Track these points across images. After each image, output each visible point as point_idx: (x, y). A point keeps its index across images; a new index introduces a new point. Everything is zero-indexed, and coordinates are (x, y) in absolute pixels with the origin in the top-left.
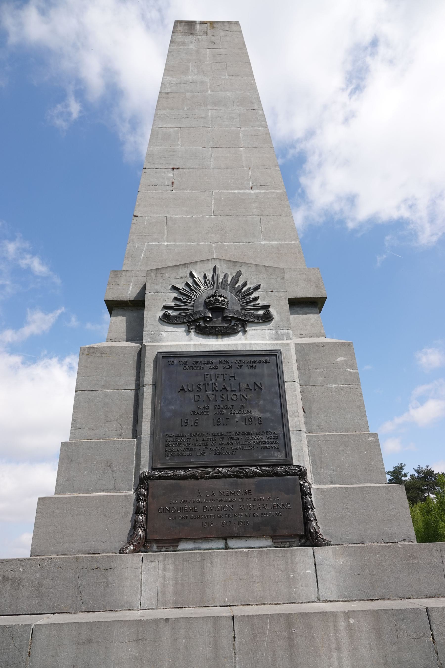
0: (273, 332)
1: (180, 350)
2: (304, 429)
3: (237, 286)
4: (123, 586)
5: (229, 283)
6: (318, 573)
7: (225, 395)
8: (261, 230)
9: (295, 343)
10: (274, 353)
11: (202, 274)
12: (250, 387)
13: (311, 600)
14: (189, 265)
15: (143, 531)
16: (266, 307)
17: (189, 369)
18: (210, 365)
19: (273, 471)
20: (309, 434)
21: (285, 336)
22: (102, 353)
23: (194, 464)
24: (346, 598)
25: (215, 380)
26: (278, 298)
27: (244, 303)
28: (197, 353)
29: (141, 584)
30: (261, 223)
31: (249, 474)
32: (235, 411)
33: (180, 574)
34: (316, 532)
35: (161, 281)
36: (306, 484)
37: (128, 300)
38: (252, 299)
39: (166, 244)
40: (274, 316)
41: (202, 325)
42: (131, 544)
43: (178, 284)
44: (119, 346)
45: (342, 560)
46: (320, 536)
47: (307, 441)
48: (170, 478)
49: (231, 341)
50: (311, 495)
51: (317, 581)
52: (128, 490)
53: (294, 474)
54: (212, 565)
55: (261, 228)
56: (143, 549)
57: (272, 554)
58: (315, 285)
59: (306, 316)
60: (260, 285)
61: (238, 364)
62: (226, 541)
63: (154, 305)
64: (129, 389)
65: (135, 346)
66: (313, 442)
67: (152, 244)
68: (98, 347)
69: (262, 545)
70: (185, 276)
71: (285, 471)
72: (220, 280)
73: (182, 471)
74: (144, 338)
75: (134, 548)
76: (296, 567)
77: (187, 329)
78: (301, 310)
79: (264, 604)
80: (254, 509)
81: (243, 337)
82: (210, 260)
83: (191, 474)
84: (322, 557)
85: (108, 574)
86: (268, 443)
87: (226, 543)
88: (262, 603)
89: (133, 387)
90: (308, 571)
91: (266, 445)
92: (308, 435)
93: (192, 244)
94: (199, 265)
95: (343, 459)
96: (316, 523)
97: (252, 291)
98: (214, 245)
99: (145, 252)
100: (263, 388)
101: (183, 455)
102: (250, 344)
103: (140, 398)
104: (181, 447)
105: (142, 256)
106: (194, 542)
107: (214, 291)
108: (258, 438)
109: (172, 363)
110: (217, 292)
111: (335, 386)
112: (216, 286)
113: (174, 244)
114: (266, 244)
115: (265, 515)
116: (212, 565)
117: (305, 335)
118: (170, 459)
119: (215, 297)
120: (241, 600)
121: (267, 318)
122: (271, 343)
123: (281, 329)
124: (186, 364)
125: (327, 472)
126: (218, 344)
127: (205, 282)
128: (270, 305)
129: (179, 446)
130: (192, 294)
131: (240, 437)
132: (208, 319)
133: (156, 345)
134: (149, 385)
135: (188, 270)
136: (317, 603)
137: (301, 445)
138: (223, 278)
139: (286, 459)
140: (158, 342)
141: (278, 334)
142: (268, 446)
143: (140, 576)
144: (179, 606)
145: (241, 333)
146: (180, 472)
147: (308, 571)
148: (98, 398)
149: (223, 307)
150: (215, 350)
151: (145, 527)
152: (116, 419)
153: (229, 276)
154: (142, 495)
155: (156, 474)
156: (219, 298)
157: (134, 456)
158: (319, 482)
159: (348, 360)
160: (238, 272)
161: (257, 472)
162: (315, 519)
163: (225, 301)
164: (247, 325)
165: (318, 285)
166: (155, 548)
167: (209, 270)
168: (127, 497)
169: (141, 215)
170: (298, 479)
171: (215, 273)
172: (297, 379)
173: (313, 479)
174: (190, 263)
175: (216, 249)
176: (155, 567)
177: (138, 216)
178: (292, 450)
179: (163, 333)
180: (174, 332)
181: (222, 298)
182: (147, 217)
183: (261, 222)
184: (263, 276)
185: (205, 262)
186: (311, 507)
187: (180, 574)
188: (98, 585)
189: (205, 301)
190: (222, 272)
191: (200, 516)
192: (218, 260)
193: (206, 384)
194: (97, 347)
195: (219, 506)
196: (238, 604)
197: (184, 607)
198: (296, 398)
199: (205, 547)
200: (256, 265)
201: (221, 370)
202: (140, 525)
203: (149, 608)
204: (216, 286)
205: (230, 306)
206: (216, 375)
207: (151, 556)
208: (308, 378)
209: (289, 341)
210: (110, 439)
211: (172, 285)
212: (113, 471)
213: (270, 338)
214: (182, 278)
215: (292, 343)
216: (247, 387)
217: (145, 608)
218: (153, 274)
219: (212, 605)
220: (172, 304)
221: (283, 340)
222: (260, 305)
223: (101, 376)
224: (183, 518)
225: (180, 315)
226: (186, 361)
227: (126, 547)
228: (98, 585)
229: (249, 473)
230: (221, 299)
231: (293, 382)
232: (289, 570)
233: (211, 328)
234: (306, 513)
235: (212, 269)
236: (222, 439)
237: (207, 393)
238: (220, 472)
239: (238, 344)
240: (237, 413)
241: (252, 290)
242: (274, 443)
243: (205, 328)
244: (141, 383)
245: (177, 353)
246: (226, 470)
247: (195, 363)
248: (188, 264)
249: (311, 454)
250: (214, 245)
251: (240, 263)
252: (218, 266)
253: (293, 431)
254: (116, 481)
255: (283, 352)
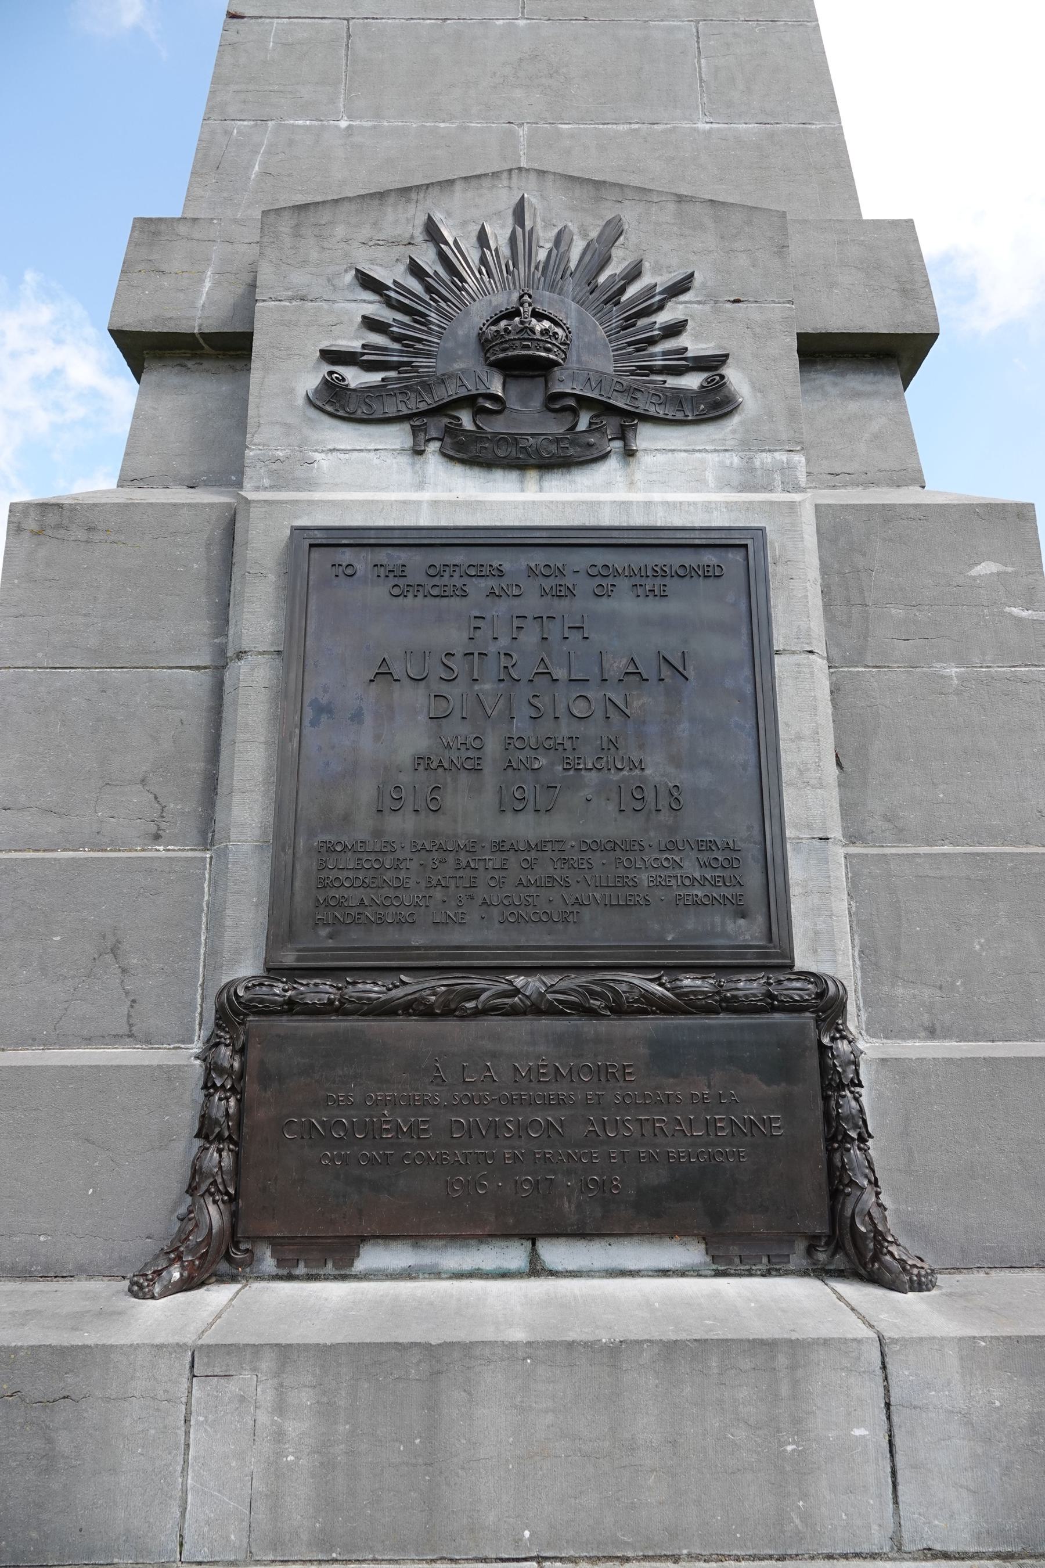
0: (736, 460)
1: (381, 523)
2: (836, 832)
3: (602, 279)
4: (115, 1470)
5: (573, 265)
6: (898, 1441)
7: (547, 699)
8: (700, 76)
9: (817, 506)
10: (737, 542)
11: (469, 229)
12: (641, 670)
13: (865, 1548)
14: (422, 195)
15: (222, 1206)
16: (712, 364)
17: (410, 595)
18: (491, 582)
19: (718, 993)
20: (853, 850)
21: (777, 477)
22: (89, 529)
23: (419, 958)
24: (1009, 1544)
25: (510, 639)
26: (758, 330)
27: (630, 344)
28: (444, 534)
29: (186, 1461)
30: (699, 52)
31: (628, 1002)
32: (581, 761)
33: (343, 1428)
34: (877, 1232)
35: (314, 255)
36: (843, 1046)
37: (196, 331)
38: (660, 329)
39: (343, 124)
40: (740, 400)
41: (467, 428)
42: (174, 1259)
43: (381, 265)
44: (153, 501)
45: (996, 1393)
46: (893, 1249)
47: (847, 878)
48: (327, 1010)
49: (576, 491)
50: (860, 1085)
51: (894, 1473)
52: (178, 1042)
53: (796, 1008)
54: (470, 1394)
55: (700, 68)
56: (223, 1267)
57: (715, 1359)
58: (895, 286)
59: (854, 407)
60: (692, 275)
61: (599, 580)
62: (534, 1244)
63: (288, 349)
64: (190, 668)
65: (212, 505)
66: (868, 881)
67: (293, 125)
68: (77, 504)
69: (666, 1265)
70: (407, 235)
71: (763, 994)
72: (542, 255)
73: (375, 984)
74: (248, 472)
75: (186, 1274)
76: (809, 1413)
77: (409, 442)
78: (835, 384)
79: (676, 1559)
80: (643, 1135)
81: (619, 479)
82: (505, 175)
83: (410, 997)
84: (917, 1375)
85: (52, 1421)
86: (703, 882)
87: (534, 1257)
88: (668, 1553)
89: (204, 660)
90: (858, 1432)
91: (695, 892)
92: (850, 855)
93: (442, 125)
94: (459, 195)
95: (977, 947)
96: (877, 1194)
97: (660, 301)
98: (523, 132)
99: (268, 152)
100: (691, 673)
101: (381, 922)
102: (648, 504)
103: (227, 699)
104: (374, 891)
105: (257, 168)
106: (416, 1246)
107: (515, 296)
108: (665, 864)
109: (349, 571)
110: (526, 298)
111: (958, 670)
112: (522, 276)
113: (375, 127)
114: (718, 129)
115: (683, 1157)
116: (470, 1394)
117: (848, 478)
118: (331, 936)
119: (517, 319)
120: (584, 1539)
121: (716, 405)
122: (727, 499)
123: (762, 451)
124: (399, 572)
125: (917, 992)
126: (524, 502)
127: (483, 261)
128: (727, 356)
129: (364, 885)
130: (430, 305)
131: (597, 858)
132: (488, 406)
133: (286, 502)
134: (260, 653)
135: (418, 214)
136: (890, 1559)
137: (825, 893)
138: (549, 245)
139: (769, 948)
140: (298, 489)
141: (753, 469)
142: (700, 894)
143: (181, 1433)
144: (334, 1555)
145: (613, 463)
146: (369, 987)
147: (858, 1432)
148: (75, 696)
149: (548, 359)
150: (512, 524)
151: (232, 1191)
152: (140, 777)
153: (575, 237)
154: (221, 1071)
155: (276, 995)
156: (534, 321)
157: (201, 917)
158: (883, 1031)
159: (1016, 573)
160: (609, 222)
161: (660, 998)
162: (873, 1179)
163: (555, 333)
164: (635, 430)
165: (908, 286)
166: (268, 1263)
167: (498, 214)
168: (168, 1074)
169: (256, 14)
170: (812, 1024)
171: (523, 226)
172: (820, 641)
173: (864, 1017)
174: (428, 186)
175: (529, 146)
176: (242, 1399)
177: (243, 17)
178: (793, 911)
179: (317, 456)
180: (363, 454)
181: (546, 324)
182: (276, 21)
183: (699, 48)
184: (703, 242)
185: (486, 183)
186: (859, 1134)
187: (341, 1428)
188: (14, 1464)
189: (480, 336)
190: (548, 224)
191: (439, 1158)
192: (533, 176)
193: (476, 655)
194: (70, 505)
195: (509, 1121)
196: (572, 1553)
197: (354, 1557)
198: (816, 715)
199: (456, 1266)
200: (680, 199)
201: (532, 603)
202: (211, 1184)
203: (218, 1559)
204: (522, 276)
205: (573, 355)
206: (515, 619)
207: (228, 1354)
208: (859, 638)
209: (796, 497)
210: (119, 850)
211: (357, 270)
212: (124, 971)
213: (723, 485)
214: (395, 243)
215: (807, 501)
216: (631, 669)
217: (200, 1559)
218: (285, 225)
219: (466, 1554)
220: (355, 345)
221: (771, 491)
222: (689, 354)
223: (85, 615)
224: (372, 1161)
225: (387, 385)
226: (400, 562)
227: (154, 1272)
228: (14, 1464)
229: (627, 998)
230: (539, 326)
231: (803, 656)
232: (781, 1425)
233: (500, 439)
234: (838, 1155)
235: (510, 211)
236: (531, 865)
237: (476, 687)
238: (517, 991)
239: (599, 503)
240: (590, 766)
241: (660, 293)
242: (724, 883)
243: (478, 436)
244: (230, 645)
245: (366, 534)
246: (538, 984)
247: (434, 572)
248: (418, 187)
249: (860, 923)
250: (523, 132)
251: (617, 190)
252: (532, 199)
253: (799, 839)
254: (136, 1006)
255: (771, 536)
